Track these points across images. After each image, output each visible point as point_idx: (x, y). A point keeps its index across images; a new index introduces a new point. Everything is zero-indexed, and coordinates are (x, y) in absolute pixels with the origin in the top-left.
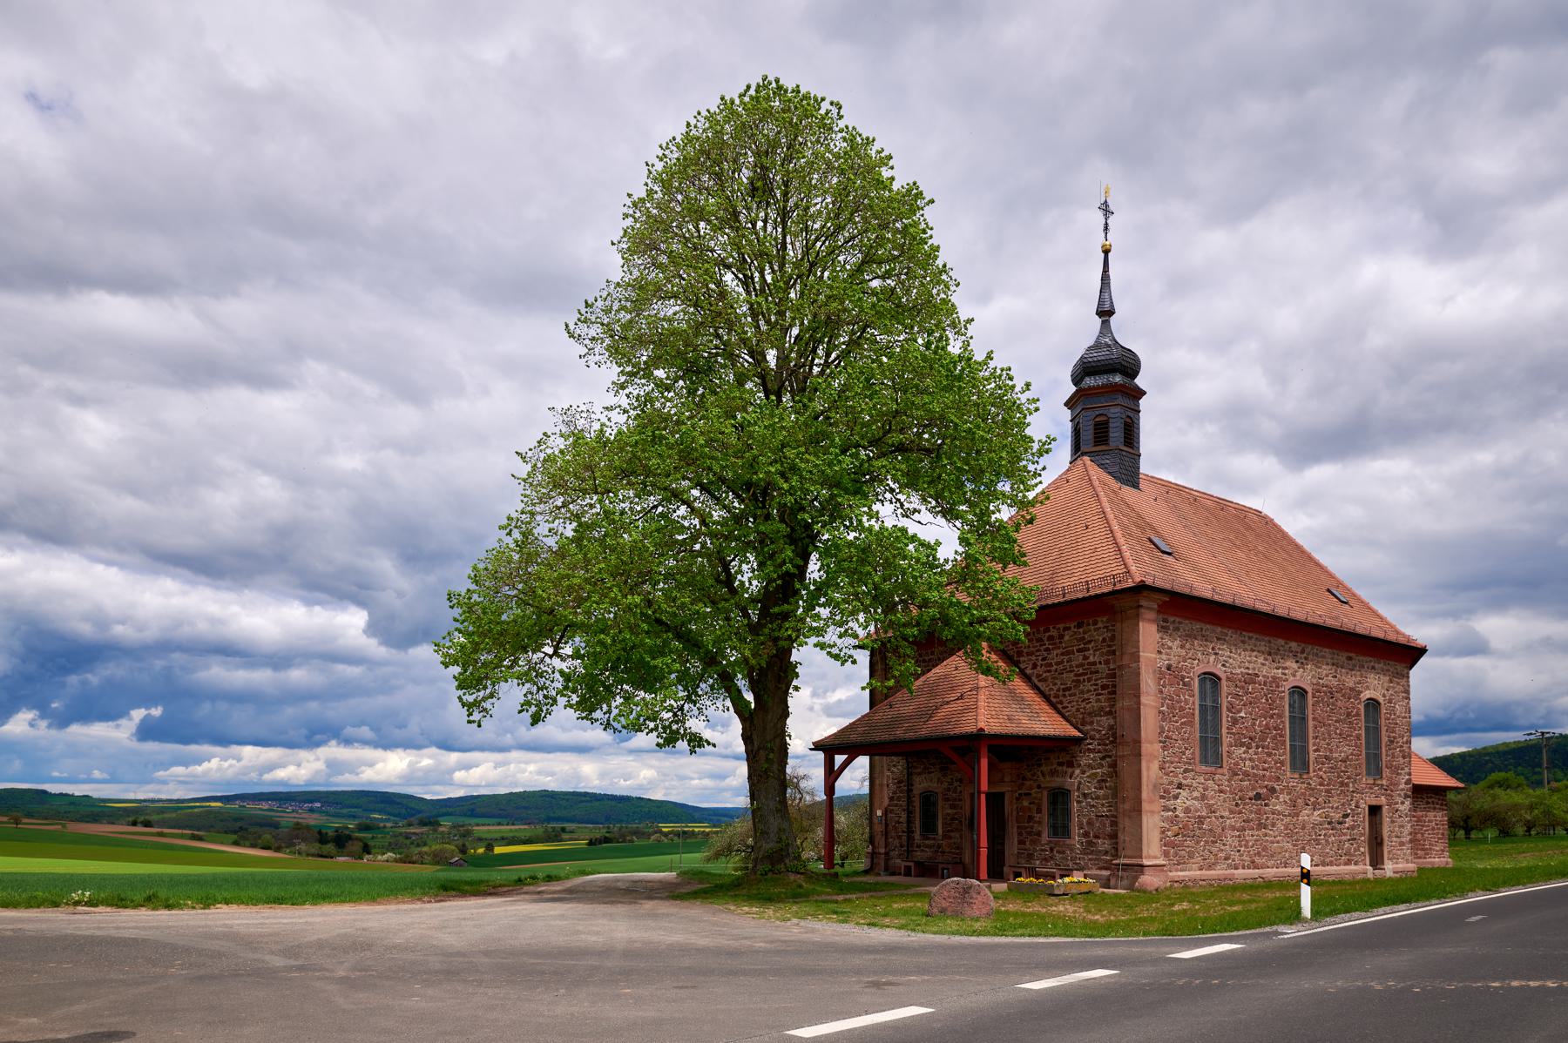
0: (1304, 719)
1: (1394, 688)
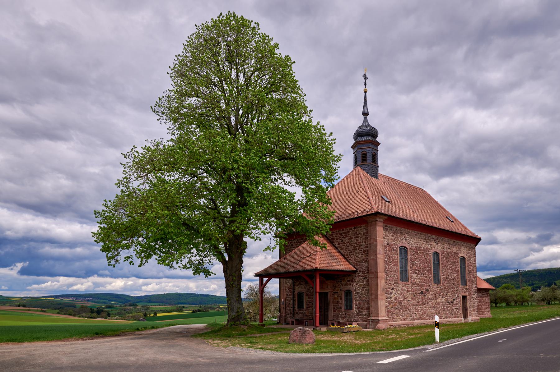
0: (438, 264)
1: (470, 253)
